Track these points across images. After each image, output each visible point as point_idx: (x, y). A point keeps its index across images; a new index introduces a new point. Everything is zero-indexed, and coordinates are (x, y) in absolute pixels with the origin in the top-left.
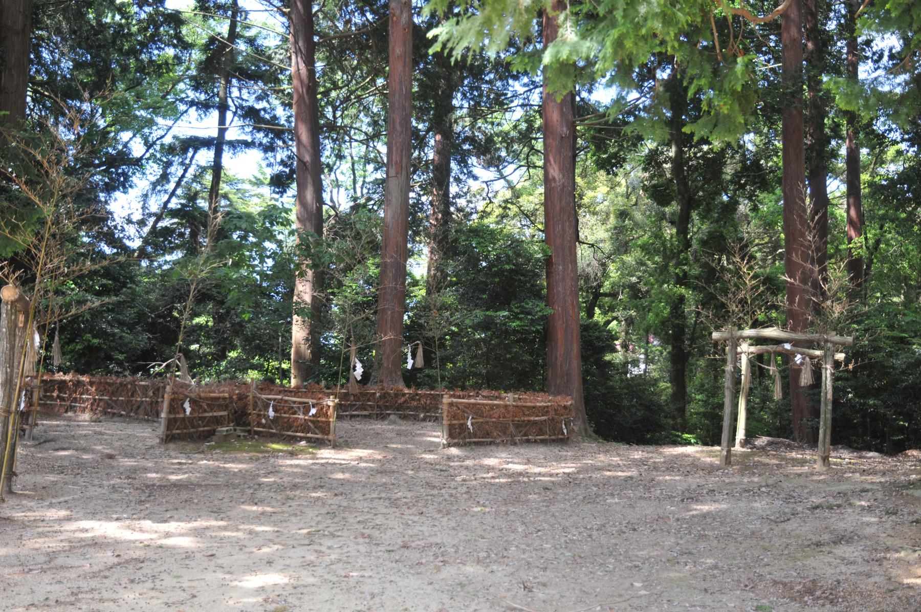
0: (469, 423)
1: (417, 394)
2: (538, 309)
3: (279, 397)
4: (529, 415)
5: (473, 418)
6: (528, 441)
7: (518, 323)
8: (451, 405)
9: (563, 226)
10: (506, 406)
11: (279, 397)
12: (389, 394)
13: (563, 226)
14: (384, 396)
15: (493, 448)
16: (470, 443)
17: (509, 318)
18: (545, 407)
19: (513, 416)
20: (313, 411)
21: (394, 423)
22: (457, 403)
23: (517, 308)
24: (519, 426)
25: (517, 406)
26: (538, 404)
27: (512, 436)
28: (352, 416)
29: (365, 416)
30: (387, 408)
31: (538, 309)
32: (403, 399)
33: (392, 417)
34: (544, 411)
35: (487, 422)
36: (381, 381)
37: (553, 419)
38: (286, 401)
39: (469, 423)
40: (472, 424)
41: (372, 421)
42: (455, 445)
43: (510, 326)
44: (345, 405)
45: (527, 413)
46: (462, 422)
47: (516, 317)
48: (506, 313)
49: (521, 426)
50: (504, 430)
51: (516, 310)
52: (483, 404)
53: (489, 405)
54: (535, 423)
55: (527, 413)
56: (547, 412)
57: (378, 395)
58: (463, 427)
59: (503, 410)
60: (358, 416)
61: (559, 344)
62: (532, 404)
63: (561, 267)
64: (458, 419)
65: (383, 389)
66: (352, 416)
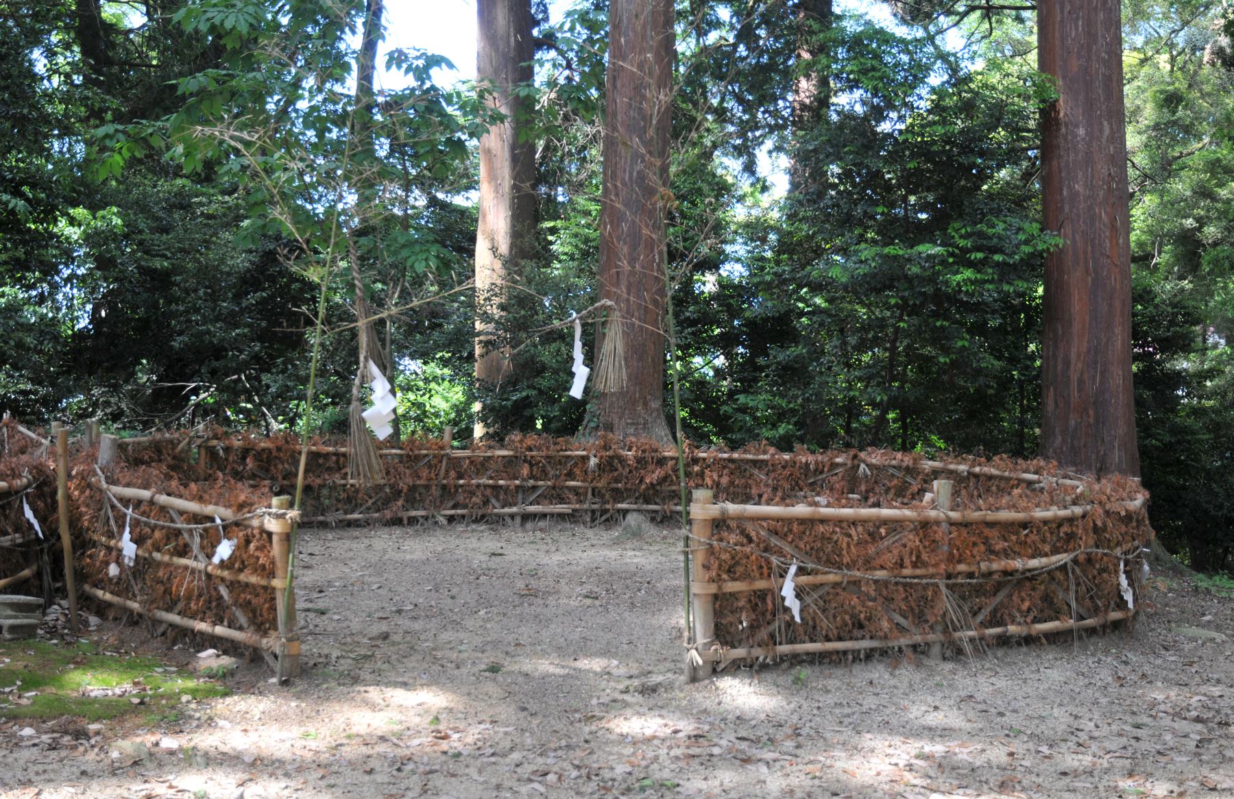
0: (788, 590)
1: (695, 461)
2: (1021, 237)
3: (146, 494)
4: (1006, 554)
5: (801, 571)
6: (1004, 641)
7: (968, 274)
8: (719, 524)
9: (1089, 24)
10: (925, 525)
11: (146, 494)
12: (622, 460)
13: (1089, 24)
14: (610, 465)
15: (878, 672)
16: (796, 660)
17: (943, 262)
18: (1060, 522)
19: (951, 559)
20: (225, 550)
21: (637, 534)
22: (740, 518)
23: (966, 236)
24: (973, 591)
25: (966, 525)
26: (1039, 514)
27: (948, 628)
28: (526, 517)
29: (561, 517)
30: (618, 495)
31: (1021, 237)
32: (658, 473)
33: (632, 519)
34: (1061, 534)
35: (856, 583)
36: (610, 427)
37: (1089, 560)
38: (163, 509)
39: (788, 590)
40: (800, 593)
41: (580, 529)
42: (735, 668)
43: (947, 283)
44: (506, 489)
45: (1000, 545)
46: (761, 584)
47: (962, 260)
48: (938, 250)
49: (978, 591)
50: (920, 610)
51: (962, 243)
52: (839, 521)
53: (864, 521)
54: (1030, 577)
55: (1000, 545)
56: (1071, 537)
57: (593, 461)
58: (764, 605)
59: (912, 540)
60: (544, 516)
61: (1076, 327)
62: (1020, 516)
63: (1081, 131)
64: (746, 577)
65: (606, 447)
66: (526, 517)
